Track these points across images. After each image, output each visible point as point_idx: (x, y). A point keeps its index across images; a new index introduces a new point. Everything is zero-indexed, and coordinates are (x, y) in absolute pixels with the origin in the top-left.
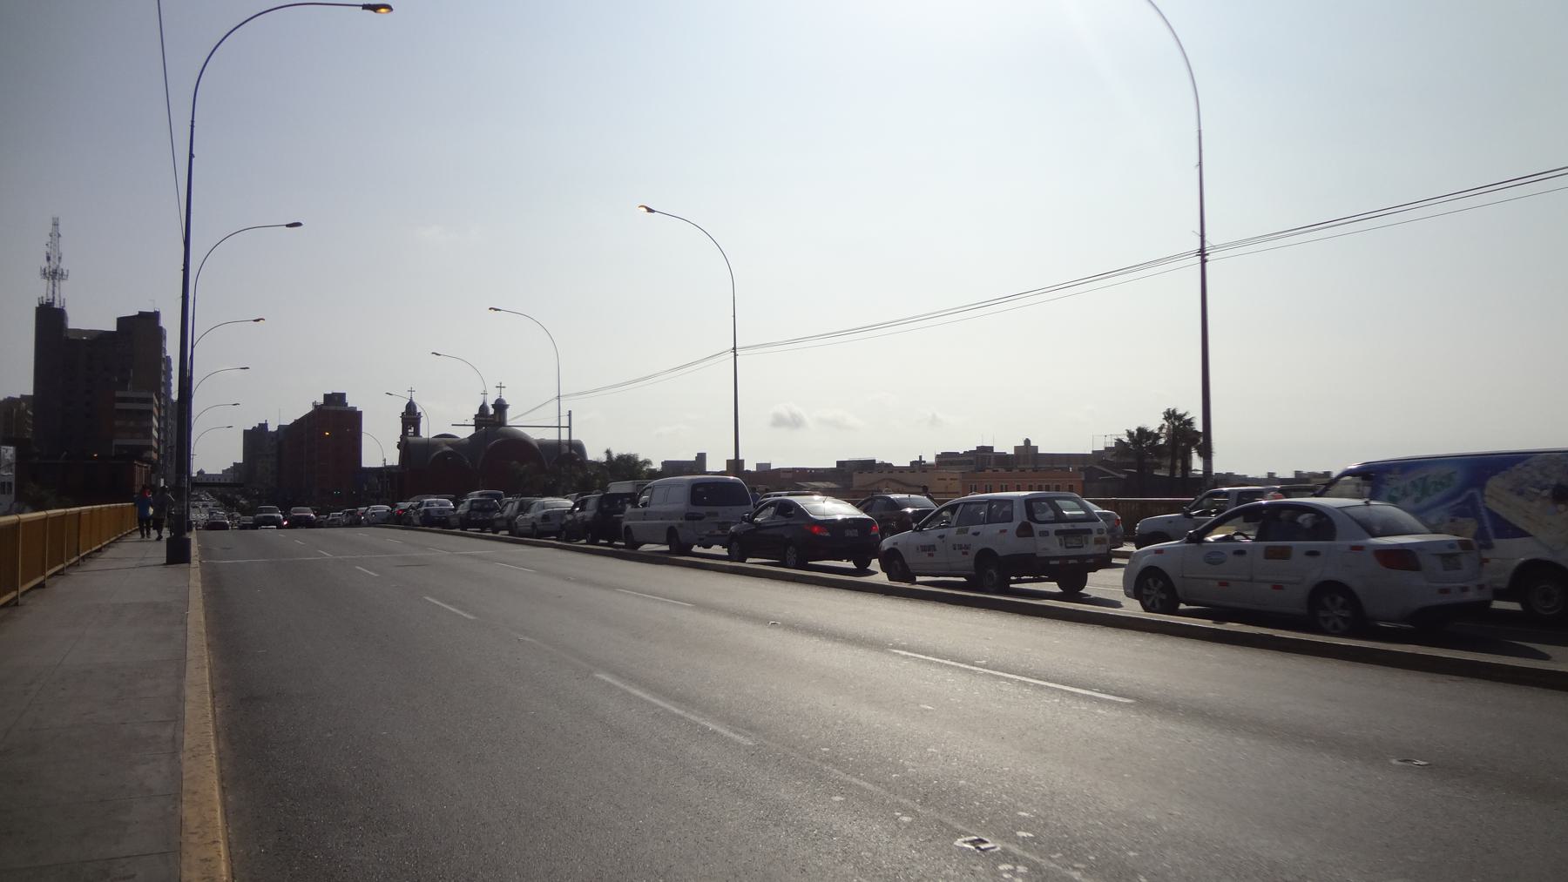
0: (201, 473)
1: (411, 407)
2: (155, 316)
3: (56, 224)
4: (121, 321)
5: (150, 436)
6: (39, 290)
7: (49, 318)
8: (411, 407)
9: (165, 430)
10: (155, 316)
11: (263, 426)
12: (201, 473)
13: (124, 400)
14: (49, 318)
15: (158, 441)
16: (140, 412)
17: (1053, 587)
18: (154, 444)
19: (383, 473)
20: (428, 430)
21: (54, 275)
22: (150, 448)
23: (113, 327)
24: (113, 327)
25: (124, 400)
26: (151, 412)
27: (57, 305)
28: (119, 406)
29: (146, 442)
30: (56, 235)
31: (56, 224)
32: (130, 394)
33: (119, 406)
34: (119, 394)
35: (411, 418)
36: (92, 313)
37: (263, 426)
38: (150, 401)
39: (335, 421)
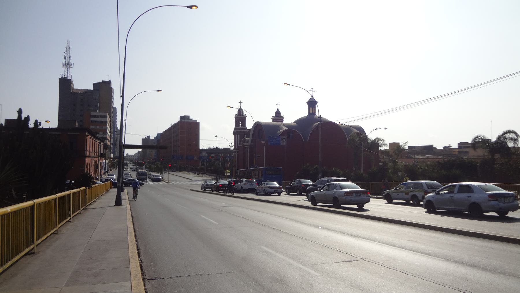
0: (127, 154)
1: (240, 111)
2: (109, 82)
3: (68, 44)
4: (95, 85)
5: (106, 133)
6: (62, 72)
7: (65, 84)
8: (240, 111)
9: (114, 138)
10: (109, 82)
11: (149, 137)
12: (127, 154)
13: (95, 116)
14: (65, 84)
15: (110, 137)
16: (102, 122)
17: (355, 206)
18: (108, 137)
19: (215, 153)
20: (249, 125)
21: (67, 65)
22: (106, 138)
23: (91, 88)
24: (91, 88)
25: (95, 116)
26: (106, 122)
27: (69, 78)
28: (92, 119)
29: (104, 136)
30: (68, 48)
31: (68, 44)
32: (98, 113)
33: (92, 119)
34: (92, 114)
35: (240, 117)
36: (83, 83)
37: (149, 137)
38: (106, 117)
39: (186, 130)
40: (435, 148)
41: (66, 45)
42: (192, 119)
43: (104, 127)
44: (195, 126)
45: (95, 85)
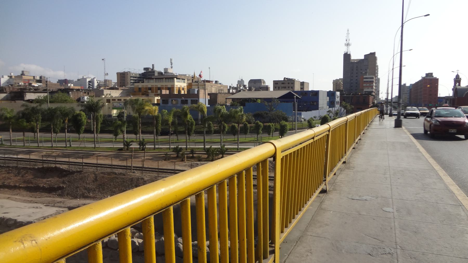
6: (344, 50)
7: (347, 56)
13: (366, 78)
14: (347, 56)
16: (370, 81)
23: (363, 58)
24: (363, 58)
25: (366, 78)
28: (365, 80)
30: (348, 34)
31: (348, 34)
33: (365, 80)
34: (365, 77)
36: (357, 55)
40: (417, 83)
41: (346, 32)
42: (336, 83)
43: (372, 85)
44: (436, 81)
45: (365, 56)
